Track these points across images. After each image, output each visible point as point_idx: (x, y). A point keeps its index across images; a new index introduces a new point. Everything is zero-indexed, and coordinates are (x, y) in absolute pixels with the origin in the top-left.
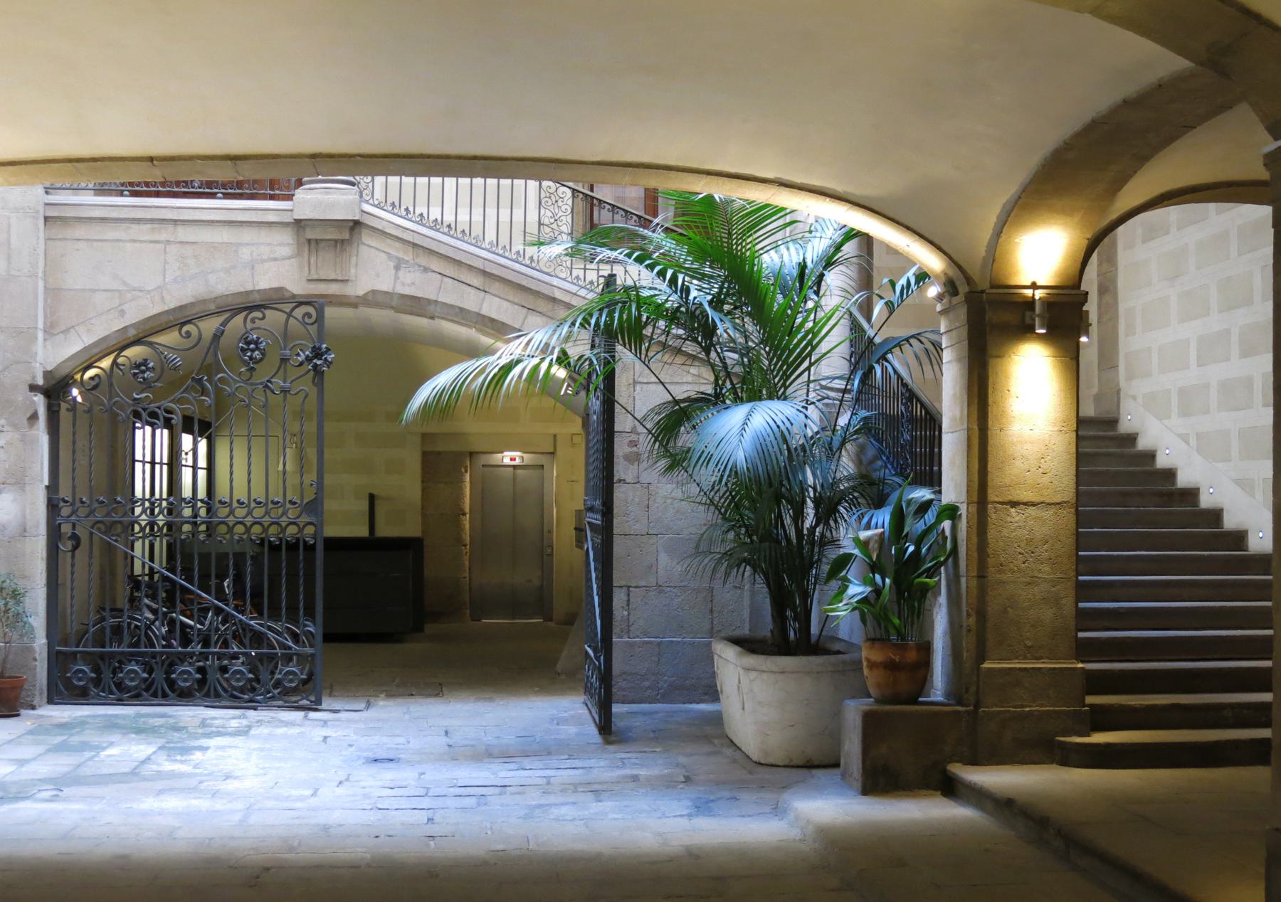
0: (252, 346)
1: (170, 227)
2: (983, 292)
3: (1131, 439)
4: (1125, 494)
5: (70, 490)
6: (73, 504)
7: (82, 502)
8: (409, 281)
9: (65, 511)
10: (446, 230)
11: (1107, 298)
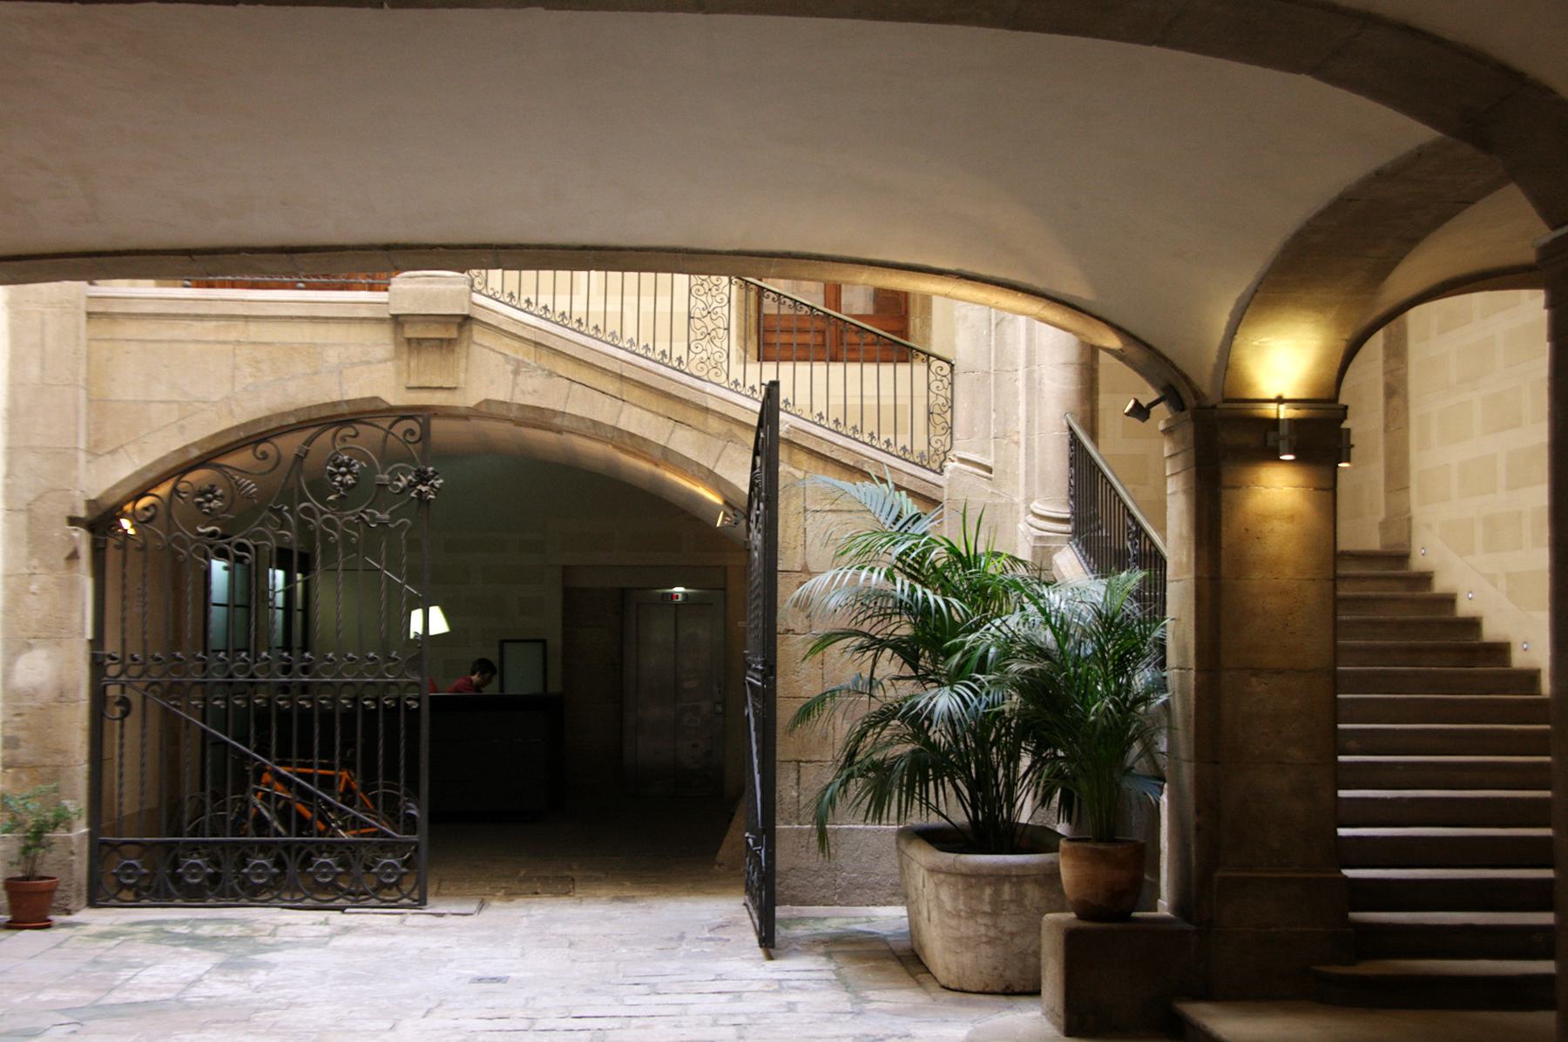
0: (343, 469)
1: (241, 324)
2: (1214, 407)
3: (1426, 579)
4: (1413, 650)
5: (119, 643)
6: (122, 661)
7: (135, 660)
8: (530, 389)
9: (113, 670)
10: (576, 326)
11: (1396, 402)
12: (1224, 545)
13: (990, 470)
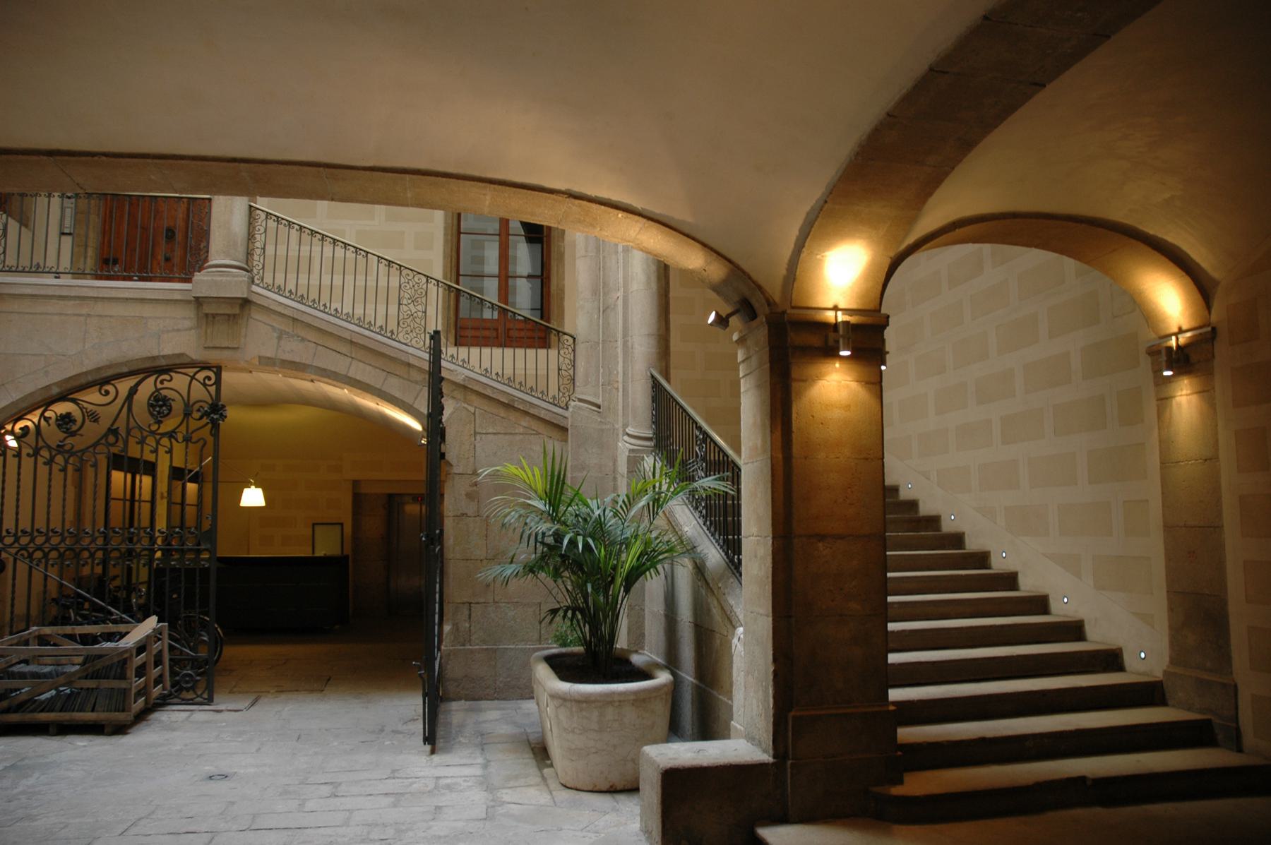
12: (794, 429)
13: (599, 407)
